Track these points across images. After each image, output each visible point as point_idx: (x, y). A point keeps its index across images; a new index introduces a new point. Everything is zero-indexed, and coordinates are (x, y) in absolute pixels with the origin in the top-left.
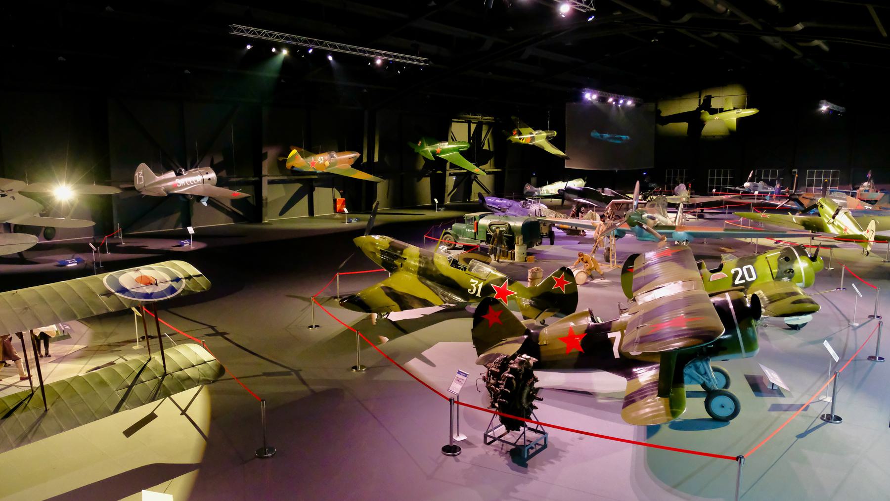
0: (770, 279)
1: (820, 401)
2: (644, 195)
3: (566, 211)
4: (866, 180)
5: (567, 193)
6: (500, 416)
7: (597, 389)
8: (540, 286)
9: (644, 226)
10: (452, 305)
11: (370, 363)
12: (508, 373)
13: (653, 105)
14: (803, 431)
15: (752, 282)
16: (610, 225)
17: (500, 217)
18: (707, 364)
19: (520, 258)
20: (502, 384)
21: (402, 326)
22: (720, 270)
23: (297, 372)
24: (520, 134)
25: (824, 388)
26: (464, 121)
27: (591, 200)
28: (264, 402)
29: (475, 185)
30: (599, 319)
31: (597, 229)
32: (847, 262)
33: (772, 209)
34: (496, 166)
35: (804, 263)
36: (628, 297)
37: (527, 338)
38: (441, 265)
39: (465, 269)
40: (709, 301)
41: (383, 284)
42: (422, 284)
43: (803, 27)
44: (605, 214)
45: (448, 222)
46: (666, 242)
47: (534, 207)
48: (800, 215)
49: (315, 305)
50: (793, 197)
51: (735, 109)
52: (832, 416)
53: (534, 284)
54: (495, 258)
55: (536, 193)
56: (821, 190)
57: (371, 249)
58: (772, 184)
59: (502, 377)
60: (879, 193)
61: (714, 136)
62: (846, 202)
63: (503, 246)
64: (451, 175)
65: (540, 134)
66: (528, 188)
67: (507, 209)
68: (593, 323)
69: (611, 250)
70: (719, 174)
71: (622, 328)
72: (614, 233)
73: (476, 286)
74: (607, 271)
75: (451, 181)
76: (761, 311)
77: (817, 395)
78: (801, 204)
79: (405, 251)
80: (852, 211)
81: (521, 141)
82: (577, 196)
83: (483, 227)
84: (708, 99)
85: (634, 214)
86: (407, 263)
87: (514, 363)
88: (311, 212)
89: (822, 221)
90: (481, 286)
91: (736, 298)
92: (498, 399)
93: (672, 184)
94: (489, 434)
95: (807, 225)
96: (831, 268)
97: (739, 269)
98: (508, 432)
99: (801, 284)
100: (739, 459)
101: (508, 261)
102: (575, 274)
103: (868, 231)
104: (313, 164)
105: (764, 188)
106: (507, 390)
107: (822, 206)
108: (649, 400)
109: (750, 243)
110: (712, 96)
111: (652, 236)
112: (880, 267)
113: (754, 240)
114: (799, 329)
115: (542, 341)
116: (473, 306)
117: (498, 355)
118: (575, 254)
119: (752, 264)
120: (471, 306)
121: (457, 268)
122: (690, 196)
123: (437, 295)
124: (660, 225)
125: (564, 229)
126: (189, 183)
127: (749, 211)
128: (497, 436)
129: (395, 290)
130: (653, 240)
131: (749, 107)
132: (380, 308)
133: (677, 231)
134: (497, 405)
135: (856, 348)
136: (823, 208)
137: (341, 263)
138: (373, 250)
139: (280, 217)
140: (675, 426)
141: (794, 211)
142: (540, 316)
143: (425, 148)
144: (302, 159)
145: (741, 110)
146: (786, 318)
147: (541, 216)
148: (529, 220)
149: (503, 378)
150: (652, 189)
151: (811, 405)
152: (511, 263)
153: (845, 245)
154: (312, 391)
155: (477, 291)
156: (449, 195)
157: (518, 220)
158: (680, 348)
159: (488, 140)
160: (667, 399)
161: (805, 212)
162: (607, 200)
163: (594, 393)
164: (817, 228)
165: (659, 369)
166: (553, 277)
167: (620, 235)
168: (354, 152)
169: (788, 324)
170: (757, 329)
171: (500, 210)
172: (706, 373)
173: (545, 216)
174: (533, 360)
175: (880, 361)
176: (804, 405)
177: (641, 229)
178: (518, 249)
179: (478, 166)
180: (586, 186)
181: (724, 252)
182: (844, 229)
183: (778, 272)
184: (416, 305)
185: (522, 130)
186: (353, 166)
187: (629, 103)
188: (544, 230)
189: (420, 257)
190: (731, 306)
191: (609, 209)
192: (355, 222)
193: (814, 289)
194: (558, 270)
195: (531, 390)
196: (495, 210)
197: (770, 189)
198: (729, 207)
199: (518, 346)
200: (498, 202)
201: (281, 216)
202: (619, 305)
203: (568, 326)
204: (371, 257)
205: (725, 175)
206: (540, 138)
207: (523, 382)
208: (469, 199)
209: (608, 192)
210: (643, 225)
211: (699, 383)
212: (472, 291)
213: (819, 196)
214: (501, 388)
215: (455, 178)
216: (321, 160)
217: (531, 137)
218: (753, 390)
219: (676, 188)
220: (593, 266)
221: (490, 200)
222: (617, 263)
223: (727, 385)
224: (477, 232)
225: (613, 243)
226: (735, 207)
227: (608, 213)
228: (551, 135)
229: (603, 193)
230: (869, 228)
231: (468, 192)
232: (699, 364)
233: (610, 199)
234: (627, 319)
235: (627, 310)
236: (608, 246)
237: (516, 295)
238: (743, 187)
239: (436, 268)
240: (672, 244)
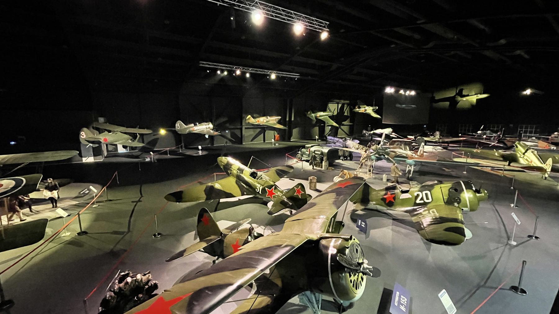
15: (429, 203)
19: (325, 168)
34: (351, 122)
43: (506, 42)
65: (369, 108)
81: (359, 111)
84: (461, 91)
88: (264, 141)
90: (261, 188)
95: (505, 158)
103: (547, 165)
105: (490, 134)
107: (517, 147)
131: (484, 93)
141: (498, 148)
152: (320, 170)
185: (361, 106)
187: (413, 93)
206: (370, 110)
208: (337, 136)
210: (385, 155)
212: (257, 190)
230: (547, 162)
238: (478, 134)
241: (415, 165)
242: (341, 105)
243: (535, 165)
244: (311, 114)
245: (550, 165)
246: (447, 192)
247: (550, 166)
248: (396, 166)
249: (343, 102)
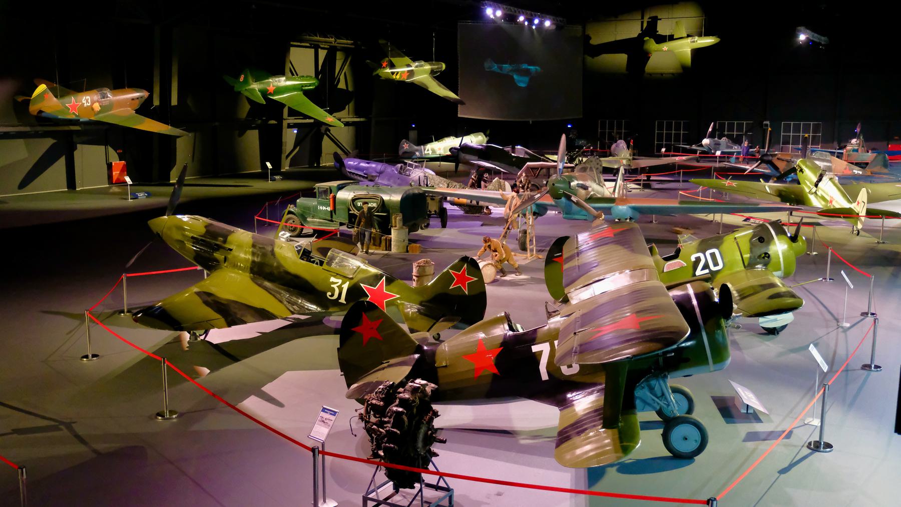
0: (741, 267)
1: (806, 424)
2: (570, 156)
3: (462, 179)
4: (854, 136)
5: (463, 153)
6: (387, 469)
7: (518, 424)
8: (432, 285)
9: (574, 199)
10: (303, 317)
11: (183, 407)
12: (397, 406)
13: (580, 28)
14: (786, 465)
16: (526, 198)
17: (369, 188)
18: (665, 382)
20: (388, 422)
21: (232, 352)
22: (676, 256)
23: (69, 426)
24: (392, 66)
25: (809, 407)
26: (308, 45)
27: (498, 163)
28: (24, 470)
29: (326, 142)
30: (519, 326)
31: (508, 203)
32: (837, 245)
33: (738, 174)
34: (357, 113)
35: (782, 245)
36: (554, 298)
37: (419, 358)
38: (285, 258)
39: (321, 263)
40: (668, 296)
41: (198, 288)
42: (257, 287)
44: (518, 183)
45: (291, 197)
46: (603, 220)
47: (417, 174)
48: (775, 182)
49: (91, 324)
50: (765, 158)
51: (688, 36)
52: (821, 443)
53: (422, 284)
54: (363, 249)
55: (417, 153)
56: (799, 149)
57: (177, 236)
58: (738, 141)
59: (388, 412)
60: (870, 154)
61: (662, 74)
62: (831, 165)
63: (373, 230)
64: (289, 126)
65: (421, 66)
66: (406, 146)
67: (376, 176)
68: (511, 333)
69: (528, 233)
70: (669, 128)
71: (551, 337)
72: (531, 209)
73: (339, 287)
74: (523, 263)
75: (290, 136)
76: (732, 307)
77: (801, 417)
78: (776, 168)
79: (230, 238)
80: (840, 178)
81: (394, 77)
82: (477, 158)
83: (344, 202)
84: (654, 22)
85: (559, 182)
86: (234, 257)
87: (404, 392)
88: (71, 184)
89: (802, 190)
90: (345, 287)
91: (700, 290)
92: (384, 444)
93: (607, 141)
94: (370, 496)
95: (784, 196)
96: (814, 253)
97: (701, 255)
98: (397, 492)
99: (779, 273)
100: (710, 502)
101: (381, 252)
102: (481, 265)
103: (858, 203)
104: (74, 107)
105: (728, 147)
106: (395, 430)
107: (801, 171)
108: (591, 434)
109: (712, 221)
111: (584, 212)
112: (872, 250)
113: (718, 217)
114: (778, 333)
115: (440, 362)
116: (336, 318)
117: (380, 383)
118: (479, 240)
119: (717, 247)
120: (332, 318)
121: (310, 261)
122: (631, 157)
123: (281, 302)
124: (595, 196)
125: (460, 205)
127: (710, 178)
128: (381, 499)
129: (218, 297)
130: (584, 217)
131: (707, 34)
132: (194, 323)
133: (618, 204)
134: (381, 453)
135: (847, 354)
136: (803, 172)
137: (131, 259)
138: (180, 238)
139: (20, 191)
140: (625, 469)
141: (767, 178)
142: (433, 329)
143: (250, 85)
144: (55, 99)
145: (696, 38)
146: (761, 320)
147: (427, 185)
148: (411, 192)
149: (389, 414)
150: (581, 147)
151: (795, 431)
152: (387, 255)
153: (831, 222)
154: (95, 451)
155: (340, 294)
156: (287, 157)
157: (395, 192)
158: (634, 356)
159: (345, 73)
160: (616, 431)
161: (781, 178)
162: (520, 163)
163: (513, 431)
164: (796, 200)
165: (604, 391)
166: (450, 271)
167: (540, 211)
168: (139, 89)
169: (762, 327)
170: (727, 331)
171: (367, 178)
172: (663, 394)
173: (433, 186)
174: (430, 387)
175: (876, 370)
176: (785, 431)
177: (568, 202)
178: (396, 234)
179: (331, 112)
180: (488, 142)
181: (678, 233)
182: (829, 200)
183: (750, 258)
184: (249, 317)
185: (394, 60)
186: (138, 111)
187: (547, 24)
188: (433, 207)
189: (254, 246)
190: (695, 302)
191: (522, 175)
192: (143, 198)
193: (794, 280)
194: (457, 261)
195: (429, 429)
196: (359, 178)
197: (736, 148)
198: (684, 173)
199: (407, 370)
201: (22, 190)
202: (546, 306)
203: (477, 339)
204: (176, 247)
205: (678, 128)
207: (417, 418)
208: (319, 163)
209: (520, 151)
210: (571, 197)
211: (654, 408)
212: (332, 295)
213: (797, 157)
214: (388, 429)
215: (296, 132)
216: (87, 102)
217: (408, 71)
218: (722, 415)
219: (614, 146)
220: (504, 256)
221: (352, 163)
222: (536, 251)
223: (690, 410)
224: (334, 211)
225: (531, 223)
226: (690, 172)
227: (521, 182)
228: (438, 68)
229: (514, 153)
230: (859, 198)
231: (316, 153)
232: (653, 382)
233: (524, 161)
234: (558, 325)
235: (557, 313)
236: (524, 228)
237: (398, 299)
238: (702, 146)
239: (278, 262)
240: (611, 222)
242: (326, 51)
243: (838, 206)
245: (864, 203)
247: (863, 204)
249: (333, 44)
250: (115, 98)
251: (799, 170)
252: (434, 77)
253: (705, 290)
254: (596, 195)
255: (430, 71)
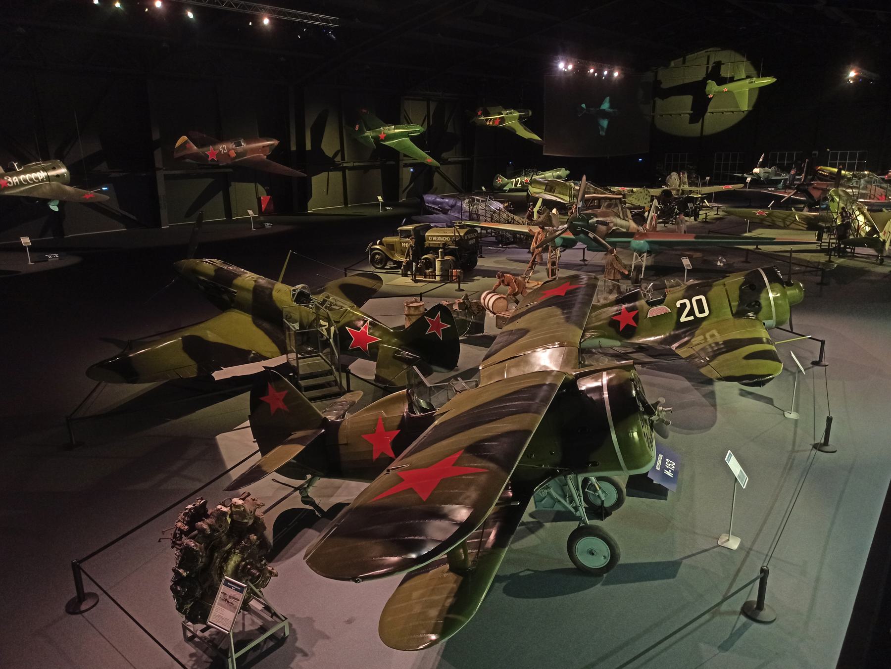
22: (660, 302)
50: (801, 187)
51: (748, 77)
65: (511, 113)
97: (687, 301)
103: (885, 233)
105: (777, 175)
110: (723, 62)
126: (25, 180)
200: (439, 201)
206: (511, 119)
216: (224, 149)
241: (649, 252)
244: (364, 133)
246: (737, 293)
248: (615, 255)
250: (248, 146)
251: (830, 199)
252: (522, 123)
253: (622, 382)
254: (619, 229)
255: (518, 118)
